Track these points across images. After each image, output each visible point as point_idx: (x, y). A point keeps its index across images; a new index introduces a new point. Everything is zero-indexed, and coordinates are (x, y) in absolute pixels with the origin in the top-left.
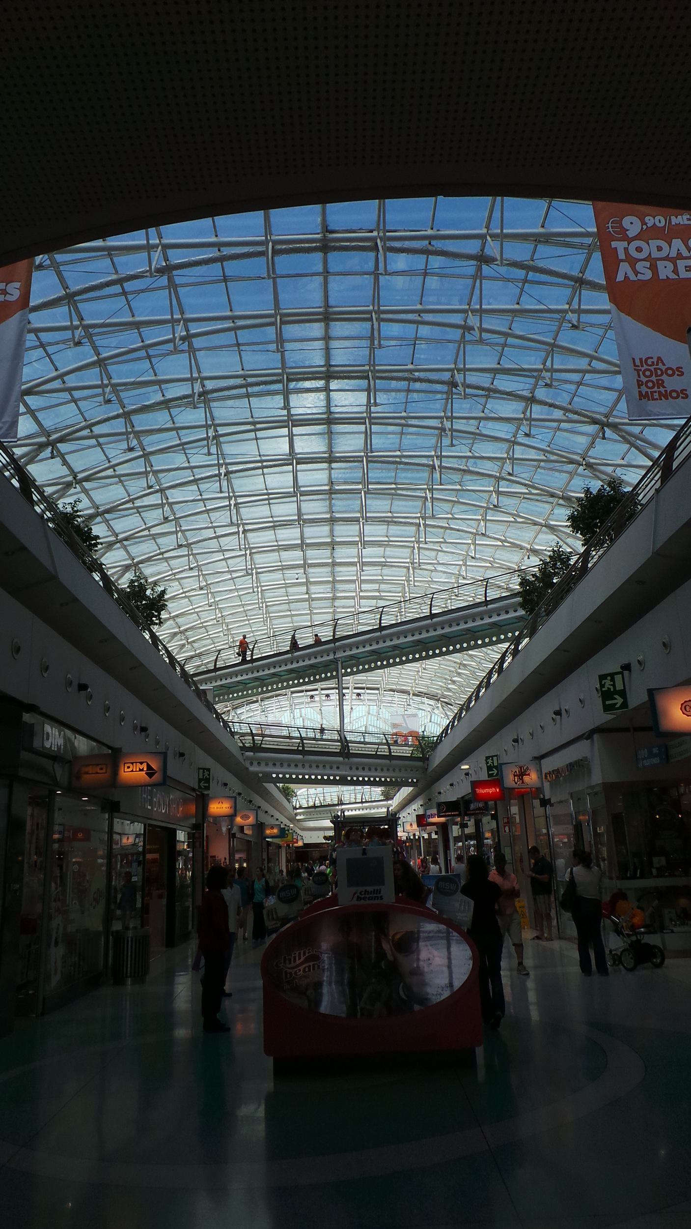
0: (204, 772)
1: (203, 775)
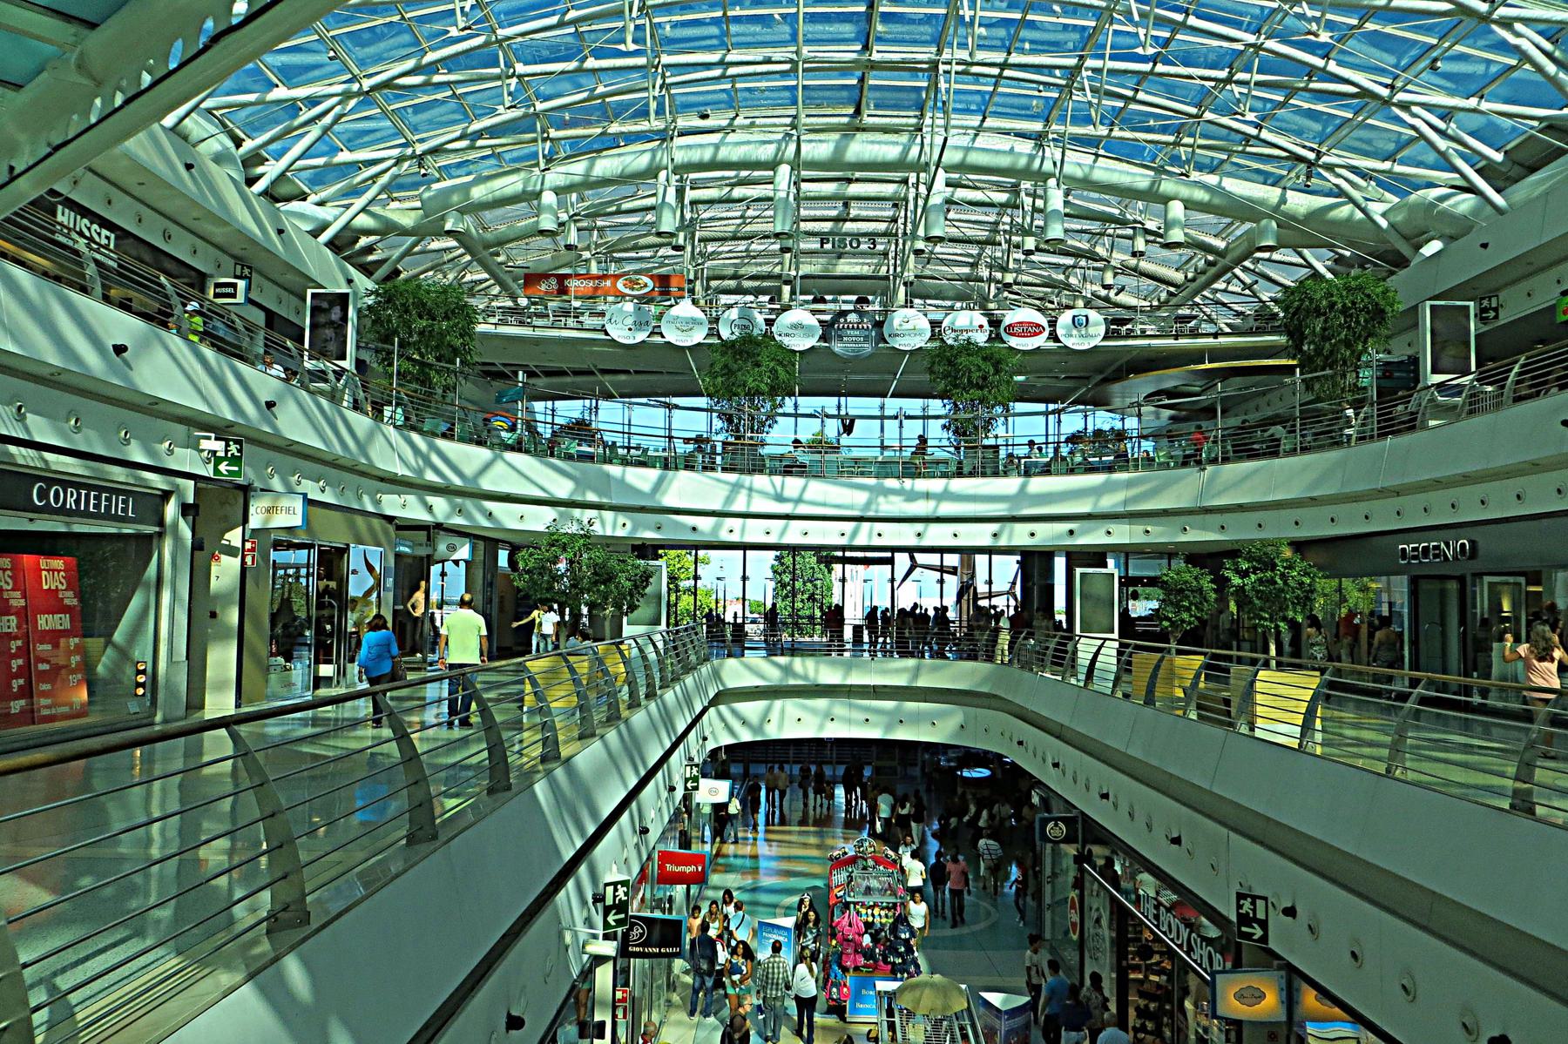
0: (616, 890)
1: (615, 897)
